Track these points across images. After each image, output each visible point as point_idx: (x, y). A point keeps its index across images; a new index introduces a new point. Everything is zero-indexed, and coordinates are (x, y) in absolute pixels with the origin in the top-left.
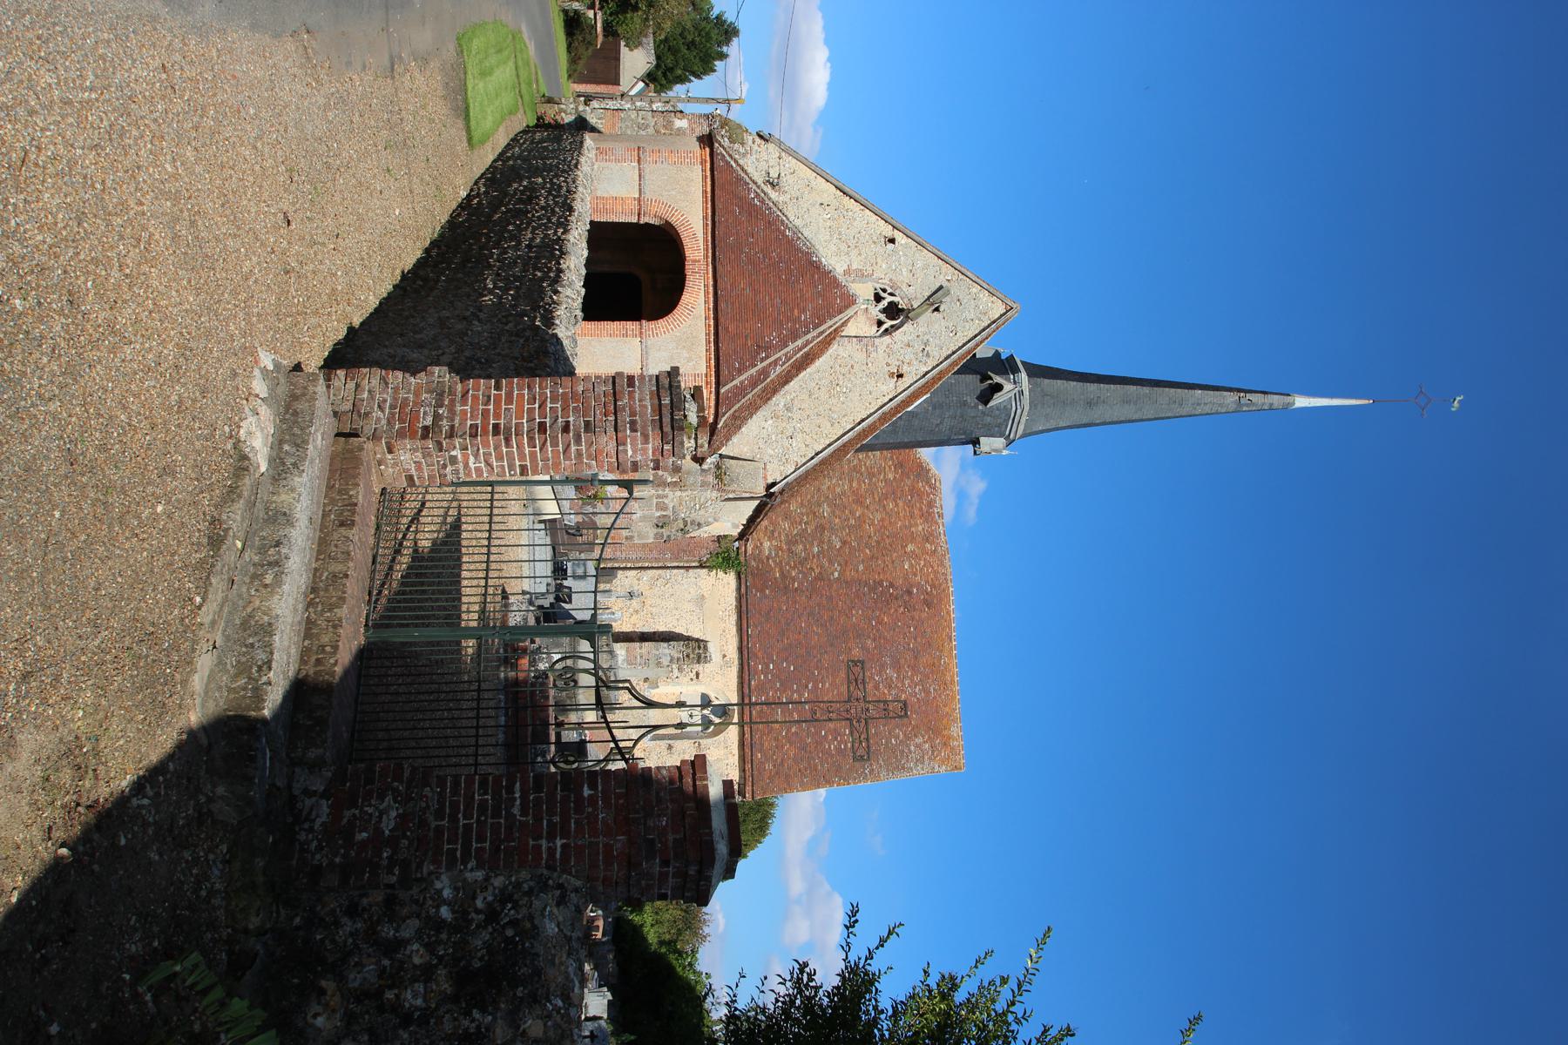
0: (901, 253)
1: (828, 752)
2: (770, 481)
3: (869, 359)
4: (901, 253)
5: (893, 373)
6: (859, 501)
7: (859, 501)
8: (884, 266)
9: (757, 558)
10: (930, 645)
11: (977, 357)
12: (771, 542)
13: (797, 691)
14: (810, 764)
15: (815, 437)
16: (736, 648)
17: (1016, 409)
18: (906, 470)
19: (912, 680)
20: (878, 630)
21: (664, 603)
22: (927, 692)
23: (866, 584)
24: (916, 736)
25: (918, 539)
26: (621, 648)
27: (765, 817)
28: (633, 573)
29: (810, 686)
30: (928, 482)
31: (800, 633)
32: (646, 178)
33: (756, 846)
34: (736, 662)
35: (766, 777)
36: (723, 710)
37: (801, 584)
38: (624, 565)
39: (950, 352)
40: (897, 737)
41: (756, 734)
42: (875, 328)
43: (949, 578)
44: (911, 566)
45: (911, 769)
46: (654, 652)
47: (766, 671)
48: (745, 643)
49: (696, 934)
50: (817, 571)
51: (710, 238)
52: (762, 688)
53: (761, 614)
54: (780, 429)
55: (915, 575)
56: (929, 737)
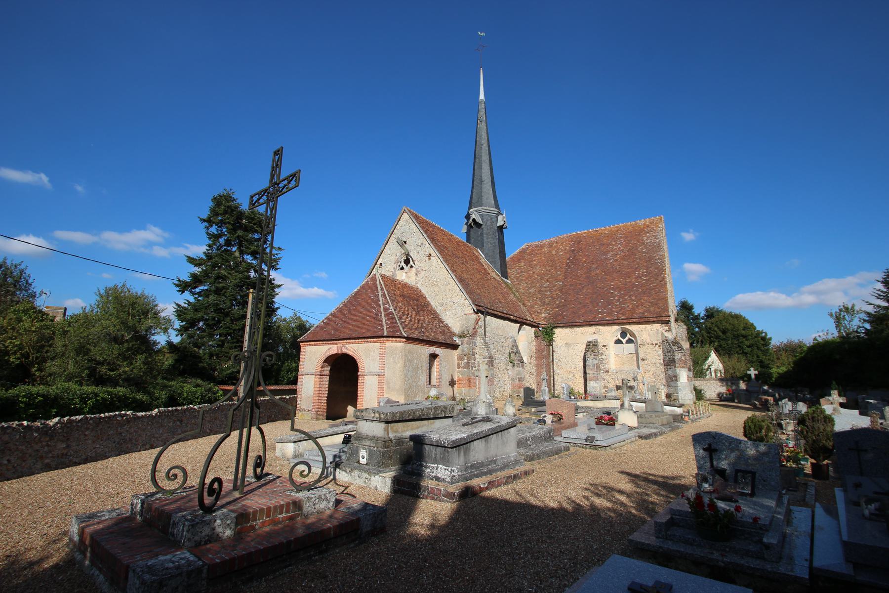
2: (472, 311)
5: (429, 258)
6: (531, 276)
7: (531, 276)
9: (548, 318)
13: (614, 297)
14: (653, 289)
15: (454, 292)
19: (614, 245)
22: (621, 237)
24: (643, 240)
27: (731, 316)
28: (556, 377)
29: (612, 291)
30: (527, 248)
31: (586, 298)
34: (597, 327)
36: (623, 334)
38: (552, 381)
40: (642, 249)
42: (413, 268)
43: (569, 234)
44: (562, 251)
45: (660, 240)
46: (591, 367)
47: (602, 313)
48: (587, 323)
50: (558, 292)
51: (330, 342)
52: (611, 314)
55: (566, 249)
56: (644, 234)
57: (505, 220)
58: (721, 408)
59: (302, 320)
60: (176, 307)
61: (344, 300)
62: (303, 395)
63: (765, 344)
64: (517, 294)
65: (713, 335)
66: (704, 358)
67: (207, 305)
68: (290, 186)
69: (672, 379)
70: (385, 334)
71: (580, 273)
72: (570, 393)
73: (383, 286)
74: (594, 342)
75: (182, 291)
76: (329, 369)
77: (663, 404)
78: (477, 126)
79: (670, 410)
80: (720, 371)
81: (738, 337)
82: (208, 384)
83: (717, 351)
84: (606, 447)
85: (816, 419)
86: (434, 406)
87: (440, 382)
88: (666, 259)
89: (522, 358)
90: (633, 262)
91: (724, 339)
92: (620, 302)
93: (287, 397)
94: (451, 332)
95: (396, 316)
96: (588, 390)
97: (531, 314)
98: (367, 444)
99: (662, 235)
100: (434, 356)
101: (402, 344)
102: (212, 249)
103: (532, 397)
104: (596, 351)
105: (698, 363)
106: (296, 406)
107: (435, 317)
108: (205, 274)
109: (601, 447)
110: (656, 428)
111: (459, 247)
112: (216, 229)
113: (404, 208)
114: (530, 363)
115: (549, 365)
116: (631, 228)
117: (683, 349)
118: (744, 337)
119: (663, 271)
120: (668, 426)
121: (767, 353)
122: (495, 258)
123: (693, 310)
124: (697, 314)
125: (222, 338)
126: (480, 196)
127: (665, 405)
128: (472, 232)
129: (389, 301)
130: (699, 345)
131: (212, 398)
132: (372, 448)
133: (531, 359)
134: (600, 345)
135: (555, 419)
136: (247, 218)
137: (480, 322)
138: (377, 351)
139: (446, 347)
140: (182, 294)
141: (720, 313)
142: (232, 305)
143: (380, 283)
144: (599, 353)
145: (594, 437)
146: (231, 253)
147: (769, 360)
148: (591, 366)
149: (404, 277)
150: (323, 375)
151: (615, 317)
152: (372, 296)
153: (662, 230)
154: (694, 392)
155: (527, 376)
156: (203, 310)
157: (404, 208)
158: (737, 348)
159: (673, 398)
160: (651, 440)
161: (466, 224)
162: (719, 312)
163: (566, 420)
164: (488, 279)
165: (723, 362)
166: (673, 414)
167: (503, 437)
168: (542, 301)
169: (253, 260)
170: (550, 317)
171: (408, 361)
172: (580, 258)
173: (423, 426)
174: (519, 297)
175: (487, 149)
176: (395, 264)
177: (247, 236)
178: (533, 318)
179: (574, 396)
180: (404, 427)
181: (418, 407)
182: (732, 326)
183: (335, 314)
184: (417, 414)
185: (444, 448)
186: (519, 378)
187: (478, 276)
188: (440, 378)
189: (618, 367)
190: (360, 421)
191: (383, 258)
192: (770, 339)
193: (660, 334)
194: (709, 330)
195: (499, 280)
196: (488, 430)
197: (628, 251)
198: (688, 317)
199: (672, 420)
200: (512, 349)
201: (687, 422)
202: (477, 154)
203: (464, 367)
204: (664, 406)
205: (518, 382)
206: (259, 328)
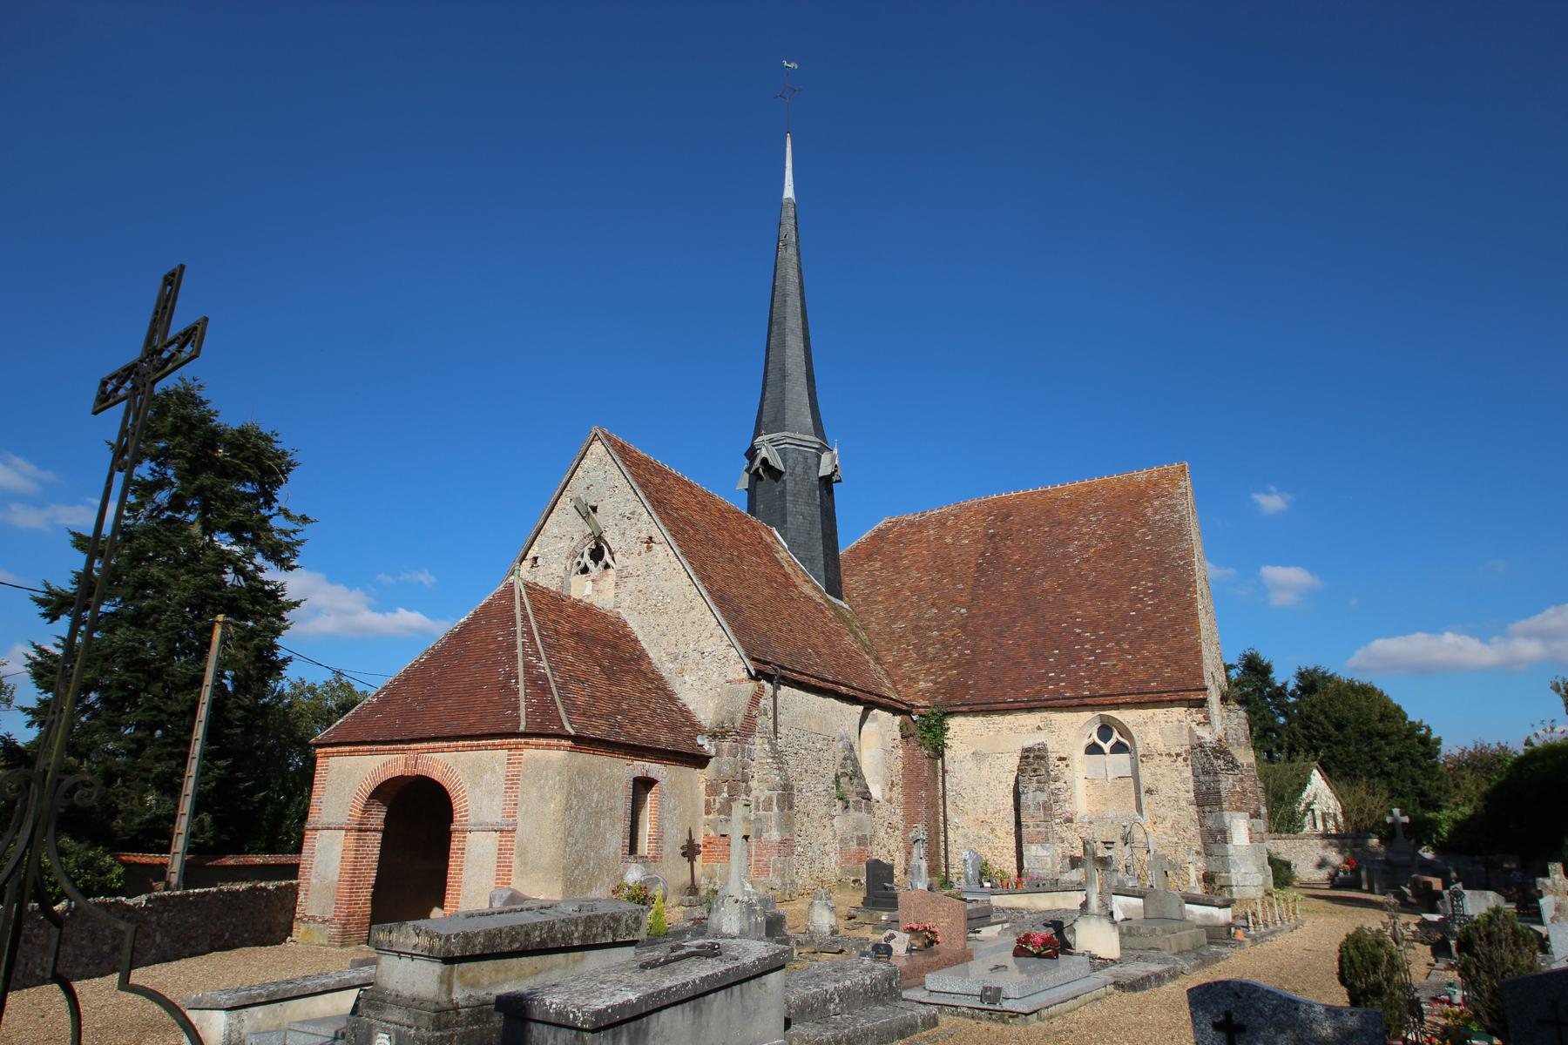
0: (546, 550)
1: (1156, 607)
2: (745, 675)
3: (634, 574)
4: (546, 550)
5: (648, 547)
6: (896, 593)
7: (896, 593)
8: (555, 566)
9: (934, 693)
10: (1048, 511)
11: (747, 487)
12: (921, 680)
14: (1168, 627)
16: (1030, 715)
17: (786, 443)
18: (875, 550)
20: (1027, 564)
21: (982, 799)
25: (942, 533)
26: (1028, 850)
28: (950, 834)
30: (890, 529)
32: (331, 821)
33: (1387, 697)
34: (1045, 714)
35: (1180, 675)
36: (1105, 731)
38: (942, 844)
39: (631, 491)
40: (1145, 534)
41: (1127, 688)
42: (610, 571)
43: (983, 499)
44: (966, 537)
46: (1031, 811)
47: (1057, 681)
50: (957, 630)
51: (387, 747)
52: (1075, 684)
53: (993, 689)
54: (694, 666)
55: (977, 532)
56: (1146, 502)
57: (837, 462)
58: (1329, 905)
59: (352, 692)
60: (33, 654)
61: (433, 644)
62: (314, 881)
63: (1428, 753)
64: (862, 635)
65: (1315, 733)
66: (1296, 787)
67: (109, 651)
68: (183, 355)
69: (1215, 838)
70: (522, 728)
72: (981, 874)
73: (529, 611)
75: (53, 616)
76: (383, 815)
77: (1183, 901)
78: (777, 254)
79: (1201, 915)
81: (1370, 738)
82: (88, 849)
83: (1326, 770)
84: (1026, 1015)
85: (1496, 937)
86: (584, 914)
87: (659, 848)
88: (1196, 559)
89: (867, 787)
90: (1125, 563)
92: (1097, 656)
93: (271, 886)
94: (693, 725)
95: (553, 685)
96: (1025, 865)
97: (895, 683)
98: (394, 1018)
100: (643, 785)
101: (561, 754)
102: (135, 517)
103: (887, 885)
104: (1043, 772)
105: (1282, 798)
106: (294, 908)
108: (112, 575)
109: (1015, 1015)
110: (1165, 961)
111: (725, 522)
112: (151, 469)
113: (595, 429)
114: (890, 801)
115: (934, 805)
116: (1118, 487)
118: (1383, 736)
120: (1193, 955)
121: (1433, 773)
122: (813, 551)
123: (1271, 676)
124: (1279, 685)
125: (140, 735)
127: (1187, 903)
128: (760, 486)
129: (540, 647)
130: (1283, 756)
131: (93, 885)
132: (405, 1029)
133: (891, 790)
135: (918, 943)
136: (230, 445)
137: (762, 701)
138: (501, 770)
140: (51, 622)
141: (1329, 682)
142: (173, 652)
143: (522, 603)
144: (1049, 775)
145: (999, 990)
146: (181, 526)
147: (1439, 789)
149: (588, 591)
150: (366, 831)
152: (500, 636)
154: (1270, 868)
155: (882, 833)
156: (99, 664)
157: (595, 429)
158: (1367, 762)
159: (1218, 883)
160: (1145, 992)
161: (748, 470)
163: (944, 944)
164: (792, 599)
165: (1340, 796)
166: (1209, 923)
167: (747, 997)
168: (921, 652)
169: (232, 544)
171: (576, 795)
172: (1006, 554)
173: (550, 969)
174: (868, 643)
175: (799, 304)
176: (567, 558)
177: (223, 488)
178: (898, 692)
179: (989, 881)
180: (497, 972)
181: (542, 919)
182: (1356, 712)
183: (408, 678)
184: (536, 937)
185: (574, 1032)
186: (858, 838)
187: (767, 591)
188: (658, 838)
189: (1094, 809)
190: (384, 957)
191: (540, 546)
192: (1438, 741)
193: (1186, 731)
194: (1306, 721)
195: (819, 601)
196: (703, 980)
197: (1113, 539)
198: (1261, 691)
199: (1206, 940)
200: (843, 766)
201: (1241, 943)
203: (720, 812)
204: (1188, 906)
205: (855, 847)
206: (62, 710)
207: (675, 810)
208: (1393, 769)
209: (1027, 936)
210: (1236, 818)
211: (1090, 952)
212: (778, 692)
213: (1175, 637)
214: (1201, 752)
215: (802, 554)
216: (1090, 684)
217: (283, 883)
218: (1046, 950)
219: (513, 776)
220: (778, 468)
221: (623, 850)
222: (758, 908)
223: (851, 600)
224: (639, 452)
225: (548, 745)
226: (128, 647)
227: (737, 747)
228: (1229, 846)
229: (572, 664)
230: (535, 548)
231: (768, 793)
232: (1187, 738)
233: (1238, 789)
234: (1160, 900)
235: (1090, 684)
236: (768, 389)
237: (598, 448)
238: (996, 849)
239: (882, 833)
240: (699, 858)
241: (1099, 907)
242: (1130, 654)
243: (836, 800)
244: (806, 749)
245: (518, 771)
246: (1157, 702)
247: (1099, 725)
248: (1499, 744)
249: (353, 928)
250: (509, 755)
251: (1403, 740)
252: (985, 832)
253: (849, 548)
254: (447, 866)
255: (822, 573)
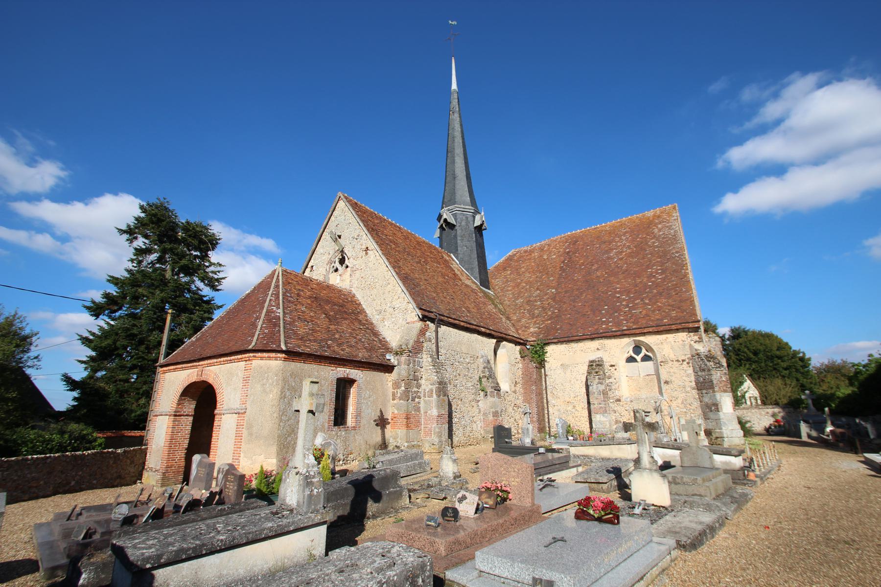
1: (663, 280)
7: (518, 285)
9: (538, 334)
14: (672, 289)
19: (618, 242)
20: (587, 264)
22: (626, 232)
23: (561, 274)
24: (653, 233)
29: (618, 295)
30: (515, 255)
33: (780, 339)
35: (682, 315)
36: (637, 349)
37: (556, 308)
38: (546, 415)
39: (358, 225)
40: (654, 243)
41: (649, 324)
43: (563, 235)
44: (554, 255)
46: (596, 395)
47: (606, 323)
48: (588, 337)
49: (843, 367)
50: (550, 301)
51: (189, 365)
52: (618, 323)
62: (154, 446)
63: (804, 366)
64: (500, 307)
69: (711, 409)
71: (577, 276)
72: (568, 432)
74: (599, 361)
75: (97, 316)
76: (193, 406)
79: (721, 462)
80: (756, 399)
81: (772, 359)
83: (751, 376)
88: (686, 252)
89: (498, 384)
90: (643, 258)
91: (755, 362)
92: (630, 308)
96: (594, 426)
97: (517, 330)
99: (677, 225)
103: (507, 440)
104: (601, 373)
107: (371, 330)
113: (340, 194)
114: (515, 392)
117: (723, 366)
118: (779, 357)
119: (683, 265)
122: (472, 264)
126: (453, 193)
127: (714, 453)
133: (515, 386)
134: (607, 366)
137: (428, 334)
138: (241, 374)
139: (369, 368)
140: (96, 319)
144: (605, 375)
147: (811, 383)
148: (596, 393)
149: (338, 281)
151: (624, 327)
153: (677, 219)
155: (510, 410)
157: (340, 194)
162: (746, 332)
165: (757, 387)
170: (540, 332)
171: (290, 391)
172: (576, 260)
175: (461, 141)
178: (519, 334)
179: (572, 436)
188: (358, 415)
189: (633, 394)
191: (314, 260)
192: (809, 359)
193: (687, 347)
197: (635, 247)
200: (483, 372)
202: (449, 149)
204: (716, 457)
207: (369, 398)
208: (786, 374)
209: (588, 499)
210: (723, 396)
211: (645, 501)
212: (439, 329)
213: (677, 294)
214: (698, 358)
215: (466, 266)
216: (627, 323)
217: (132, 449)
218: (606, 514)
219: (247, 377)
220: (451, 222)
221: (329, 423)
222: (315, 480)
223: (495, 290)
224: (367, 207)
225: (269, 357)
226: (124, 328)
227: (409, 360)
228: (721, 413)
229: (303, 312)
230: (312, 261)
231: (430, 387)
232: (689, 350)
233: (724, 379)
234: (694, 454)
235: (627, 323)
236: (447, 185)
237: (342, 204)
238: (577, 417)
239: (510, 410)
240: (388, 426)
241: (650, 463)
242: (650, 305)
243: (480, 391)
244: (459, 362)
245: (249, 375)
246: (669, 330)
247: (634, 345)
248: (842, 360)
249: (171, 475)
250: (246, 365)
251: (790, 359)
252: (570, 408)
253: (494, 266)
254: (211, 436)
255: (478, 275)
